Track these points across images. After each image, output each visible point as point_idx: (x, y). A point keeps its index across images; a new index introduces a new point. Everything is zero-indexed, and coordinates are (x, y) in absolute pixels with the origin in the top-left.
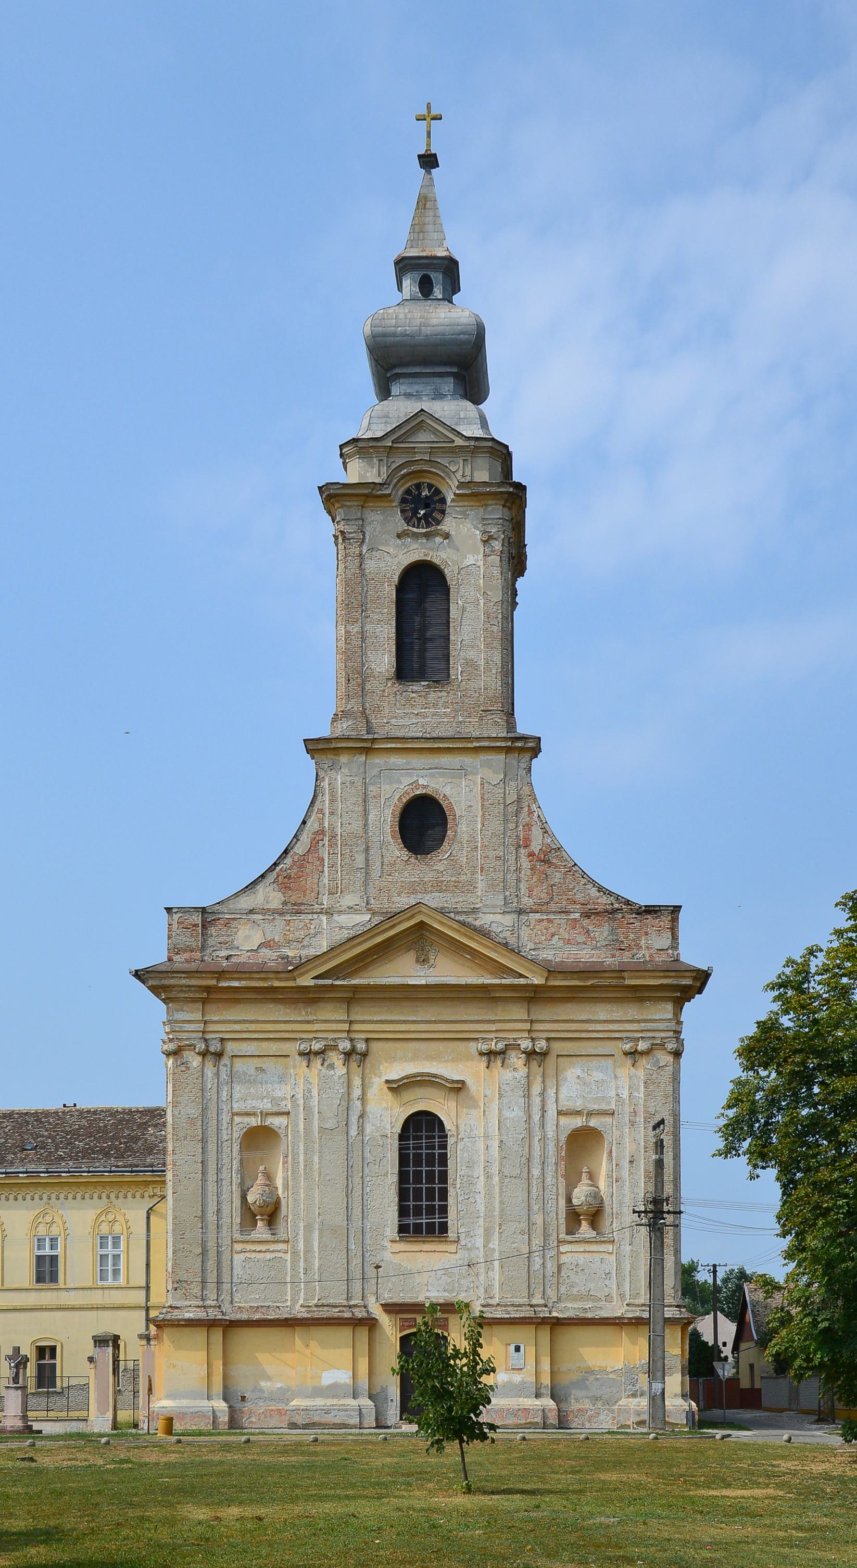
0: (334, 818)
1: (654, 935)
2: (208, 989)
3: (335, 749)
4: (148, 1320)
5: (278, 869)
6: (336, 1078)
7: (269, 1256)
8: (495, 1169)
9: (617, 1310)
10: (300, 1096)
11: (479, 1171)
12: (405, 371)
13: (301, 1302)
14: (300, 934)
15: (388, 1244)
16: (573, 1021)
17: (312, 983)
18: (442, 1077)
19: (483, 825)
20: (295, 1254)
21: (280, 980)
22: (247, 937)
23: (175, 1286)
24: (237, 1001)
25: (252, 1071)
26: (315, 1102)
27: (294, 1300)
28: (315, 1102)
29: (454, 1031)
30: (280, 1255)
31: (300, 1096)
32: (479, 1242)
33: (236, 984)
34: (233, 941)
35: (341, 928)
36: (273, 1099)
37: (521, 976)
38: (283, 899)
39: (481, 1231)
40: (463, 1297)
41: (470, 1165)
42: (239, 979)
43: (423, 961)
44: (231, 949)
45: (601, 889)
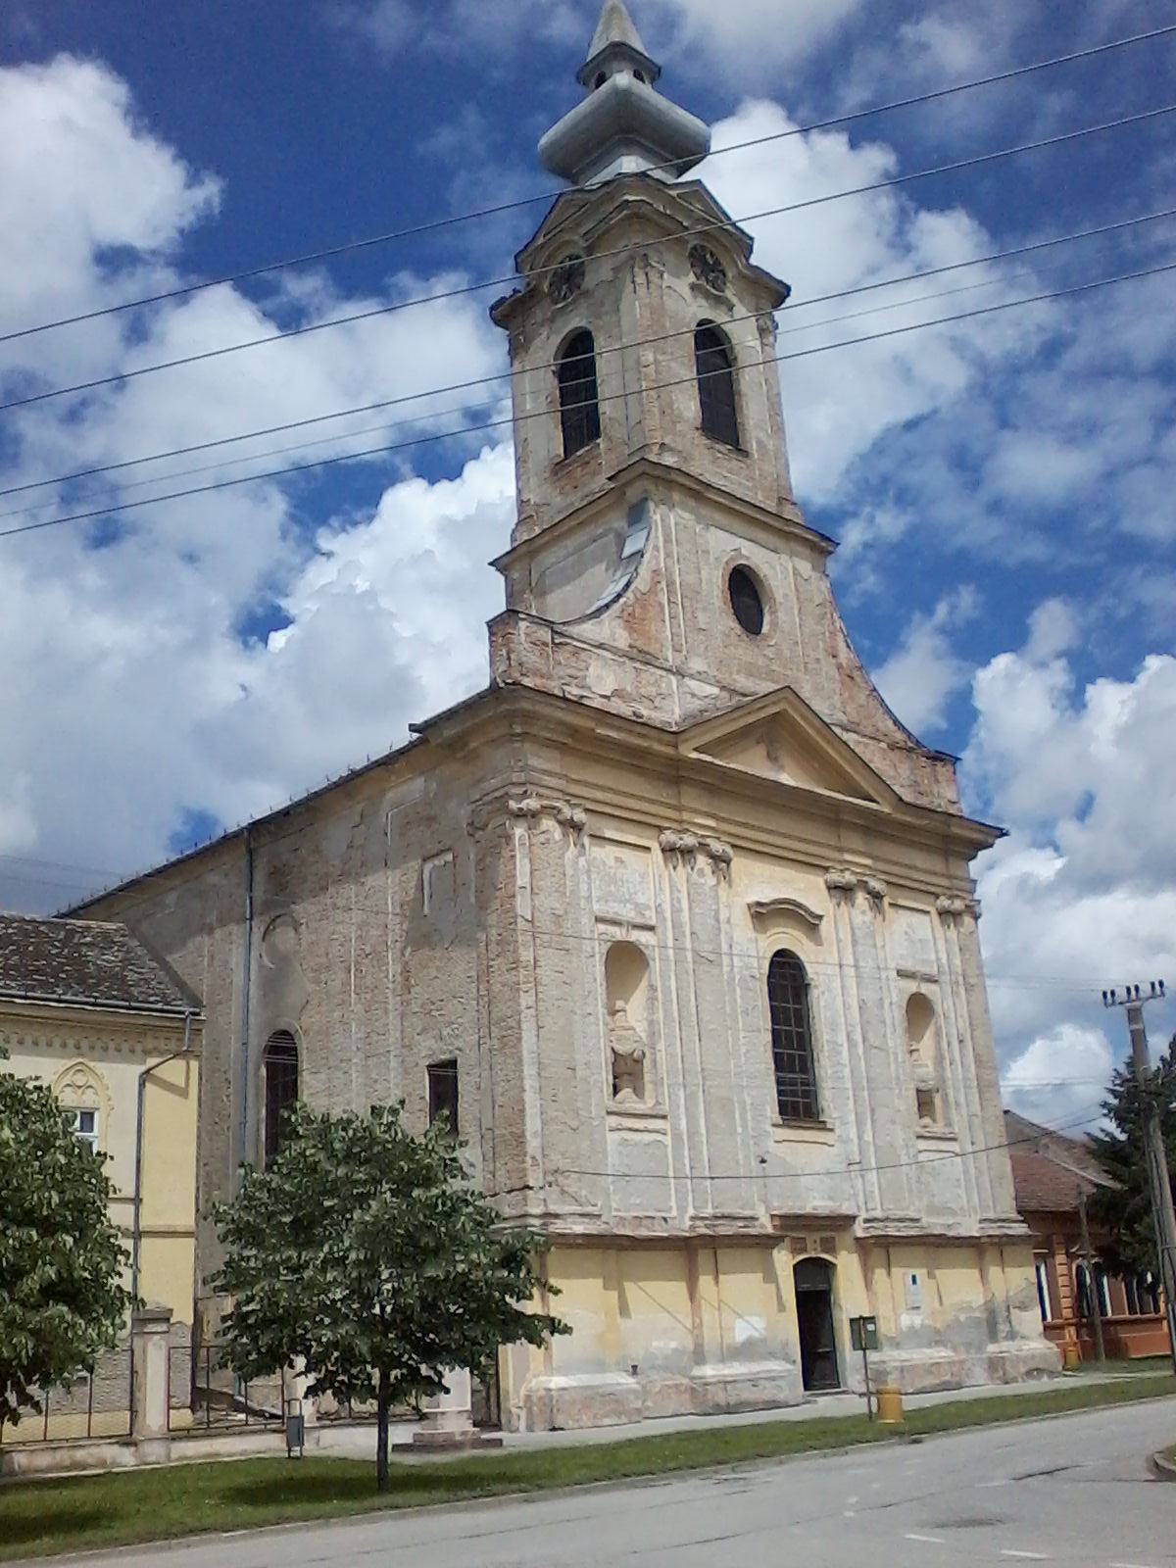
0: (669, 562)
1: (944, 784)
2: (574, 732)
3: (671, 481)
4: (137, 1201)
5: (622, 600)
6: (707, 888)
7: (648, 1137)
8: (858, 1037)
9: (971, 1228)
10: (667, 907)
11: (842, 1038)
12: (642, 141)
13: (691, 1212)
14: (652, 690)
15: (771, 1129)
16: (896, 863)
17: (694, 755)
18: (806, 910)
19: (801, 619)
20: (677, 1136)
21: (660, 741)
22: (599, 678)
23: (550, 1178)
24: (598, 759)
25: (611, 862)
26: (685, 916)
27: (682, 1209)
28: (685, 916)
29: (814, 855)
30: (659, 1137)
31: (667, 907)
32: (853, 1133)
33: (613, 734)
34: (585, 677)
35: (693, 695)
36: (637, 905)
37: (872, 800)
38: (630, 641)
39: (852, 1117)
40: (846, 1209)
41: (834, 1030)
42: (619, 729)
43: (772, 757)
44: (582, 687)
45: (896, 722)
